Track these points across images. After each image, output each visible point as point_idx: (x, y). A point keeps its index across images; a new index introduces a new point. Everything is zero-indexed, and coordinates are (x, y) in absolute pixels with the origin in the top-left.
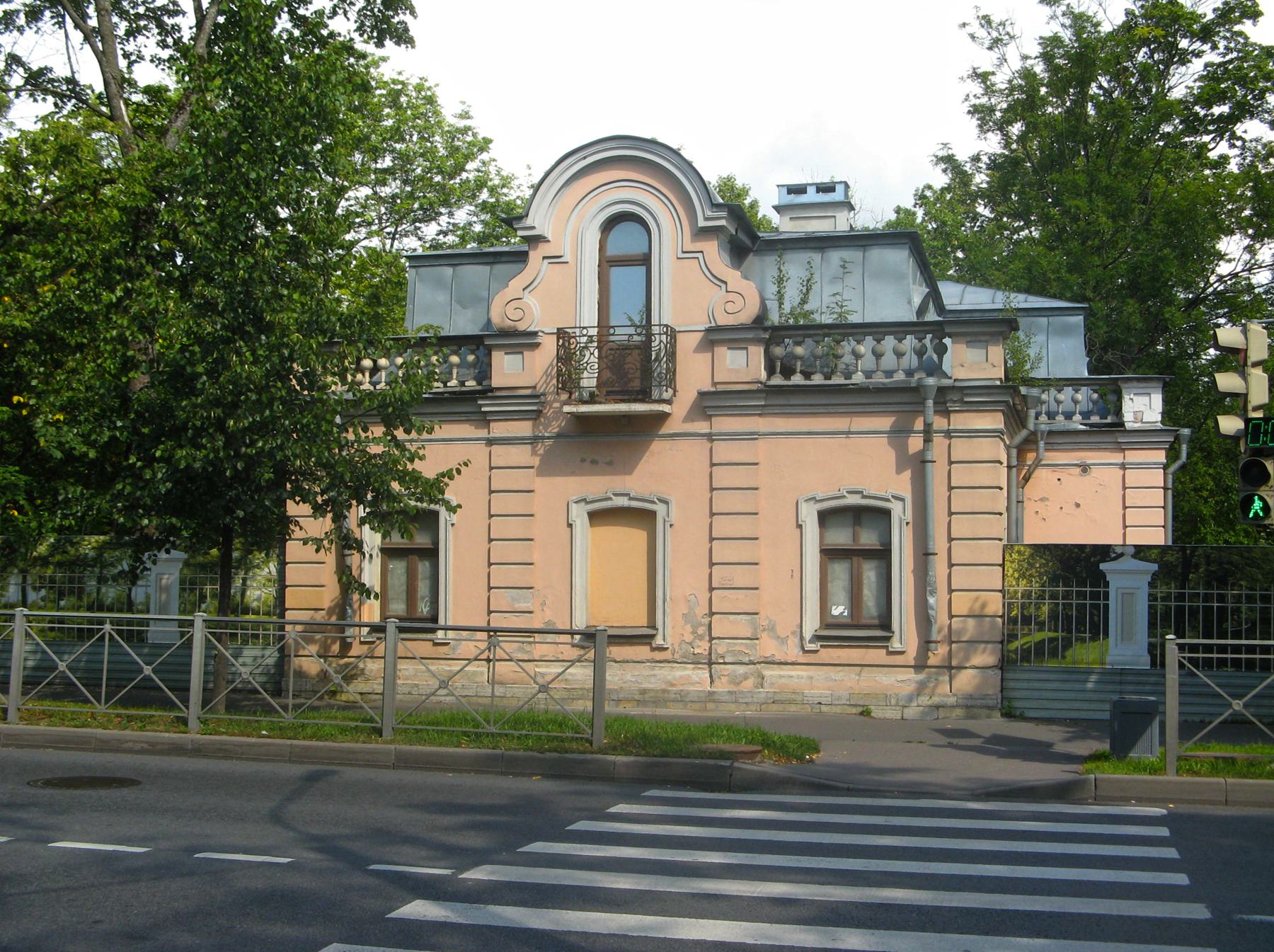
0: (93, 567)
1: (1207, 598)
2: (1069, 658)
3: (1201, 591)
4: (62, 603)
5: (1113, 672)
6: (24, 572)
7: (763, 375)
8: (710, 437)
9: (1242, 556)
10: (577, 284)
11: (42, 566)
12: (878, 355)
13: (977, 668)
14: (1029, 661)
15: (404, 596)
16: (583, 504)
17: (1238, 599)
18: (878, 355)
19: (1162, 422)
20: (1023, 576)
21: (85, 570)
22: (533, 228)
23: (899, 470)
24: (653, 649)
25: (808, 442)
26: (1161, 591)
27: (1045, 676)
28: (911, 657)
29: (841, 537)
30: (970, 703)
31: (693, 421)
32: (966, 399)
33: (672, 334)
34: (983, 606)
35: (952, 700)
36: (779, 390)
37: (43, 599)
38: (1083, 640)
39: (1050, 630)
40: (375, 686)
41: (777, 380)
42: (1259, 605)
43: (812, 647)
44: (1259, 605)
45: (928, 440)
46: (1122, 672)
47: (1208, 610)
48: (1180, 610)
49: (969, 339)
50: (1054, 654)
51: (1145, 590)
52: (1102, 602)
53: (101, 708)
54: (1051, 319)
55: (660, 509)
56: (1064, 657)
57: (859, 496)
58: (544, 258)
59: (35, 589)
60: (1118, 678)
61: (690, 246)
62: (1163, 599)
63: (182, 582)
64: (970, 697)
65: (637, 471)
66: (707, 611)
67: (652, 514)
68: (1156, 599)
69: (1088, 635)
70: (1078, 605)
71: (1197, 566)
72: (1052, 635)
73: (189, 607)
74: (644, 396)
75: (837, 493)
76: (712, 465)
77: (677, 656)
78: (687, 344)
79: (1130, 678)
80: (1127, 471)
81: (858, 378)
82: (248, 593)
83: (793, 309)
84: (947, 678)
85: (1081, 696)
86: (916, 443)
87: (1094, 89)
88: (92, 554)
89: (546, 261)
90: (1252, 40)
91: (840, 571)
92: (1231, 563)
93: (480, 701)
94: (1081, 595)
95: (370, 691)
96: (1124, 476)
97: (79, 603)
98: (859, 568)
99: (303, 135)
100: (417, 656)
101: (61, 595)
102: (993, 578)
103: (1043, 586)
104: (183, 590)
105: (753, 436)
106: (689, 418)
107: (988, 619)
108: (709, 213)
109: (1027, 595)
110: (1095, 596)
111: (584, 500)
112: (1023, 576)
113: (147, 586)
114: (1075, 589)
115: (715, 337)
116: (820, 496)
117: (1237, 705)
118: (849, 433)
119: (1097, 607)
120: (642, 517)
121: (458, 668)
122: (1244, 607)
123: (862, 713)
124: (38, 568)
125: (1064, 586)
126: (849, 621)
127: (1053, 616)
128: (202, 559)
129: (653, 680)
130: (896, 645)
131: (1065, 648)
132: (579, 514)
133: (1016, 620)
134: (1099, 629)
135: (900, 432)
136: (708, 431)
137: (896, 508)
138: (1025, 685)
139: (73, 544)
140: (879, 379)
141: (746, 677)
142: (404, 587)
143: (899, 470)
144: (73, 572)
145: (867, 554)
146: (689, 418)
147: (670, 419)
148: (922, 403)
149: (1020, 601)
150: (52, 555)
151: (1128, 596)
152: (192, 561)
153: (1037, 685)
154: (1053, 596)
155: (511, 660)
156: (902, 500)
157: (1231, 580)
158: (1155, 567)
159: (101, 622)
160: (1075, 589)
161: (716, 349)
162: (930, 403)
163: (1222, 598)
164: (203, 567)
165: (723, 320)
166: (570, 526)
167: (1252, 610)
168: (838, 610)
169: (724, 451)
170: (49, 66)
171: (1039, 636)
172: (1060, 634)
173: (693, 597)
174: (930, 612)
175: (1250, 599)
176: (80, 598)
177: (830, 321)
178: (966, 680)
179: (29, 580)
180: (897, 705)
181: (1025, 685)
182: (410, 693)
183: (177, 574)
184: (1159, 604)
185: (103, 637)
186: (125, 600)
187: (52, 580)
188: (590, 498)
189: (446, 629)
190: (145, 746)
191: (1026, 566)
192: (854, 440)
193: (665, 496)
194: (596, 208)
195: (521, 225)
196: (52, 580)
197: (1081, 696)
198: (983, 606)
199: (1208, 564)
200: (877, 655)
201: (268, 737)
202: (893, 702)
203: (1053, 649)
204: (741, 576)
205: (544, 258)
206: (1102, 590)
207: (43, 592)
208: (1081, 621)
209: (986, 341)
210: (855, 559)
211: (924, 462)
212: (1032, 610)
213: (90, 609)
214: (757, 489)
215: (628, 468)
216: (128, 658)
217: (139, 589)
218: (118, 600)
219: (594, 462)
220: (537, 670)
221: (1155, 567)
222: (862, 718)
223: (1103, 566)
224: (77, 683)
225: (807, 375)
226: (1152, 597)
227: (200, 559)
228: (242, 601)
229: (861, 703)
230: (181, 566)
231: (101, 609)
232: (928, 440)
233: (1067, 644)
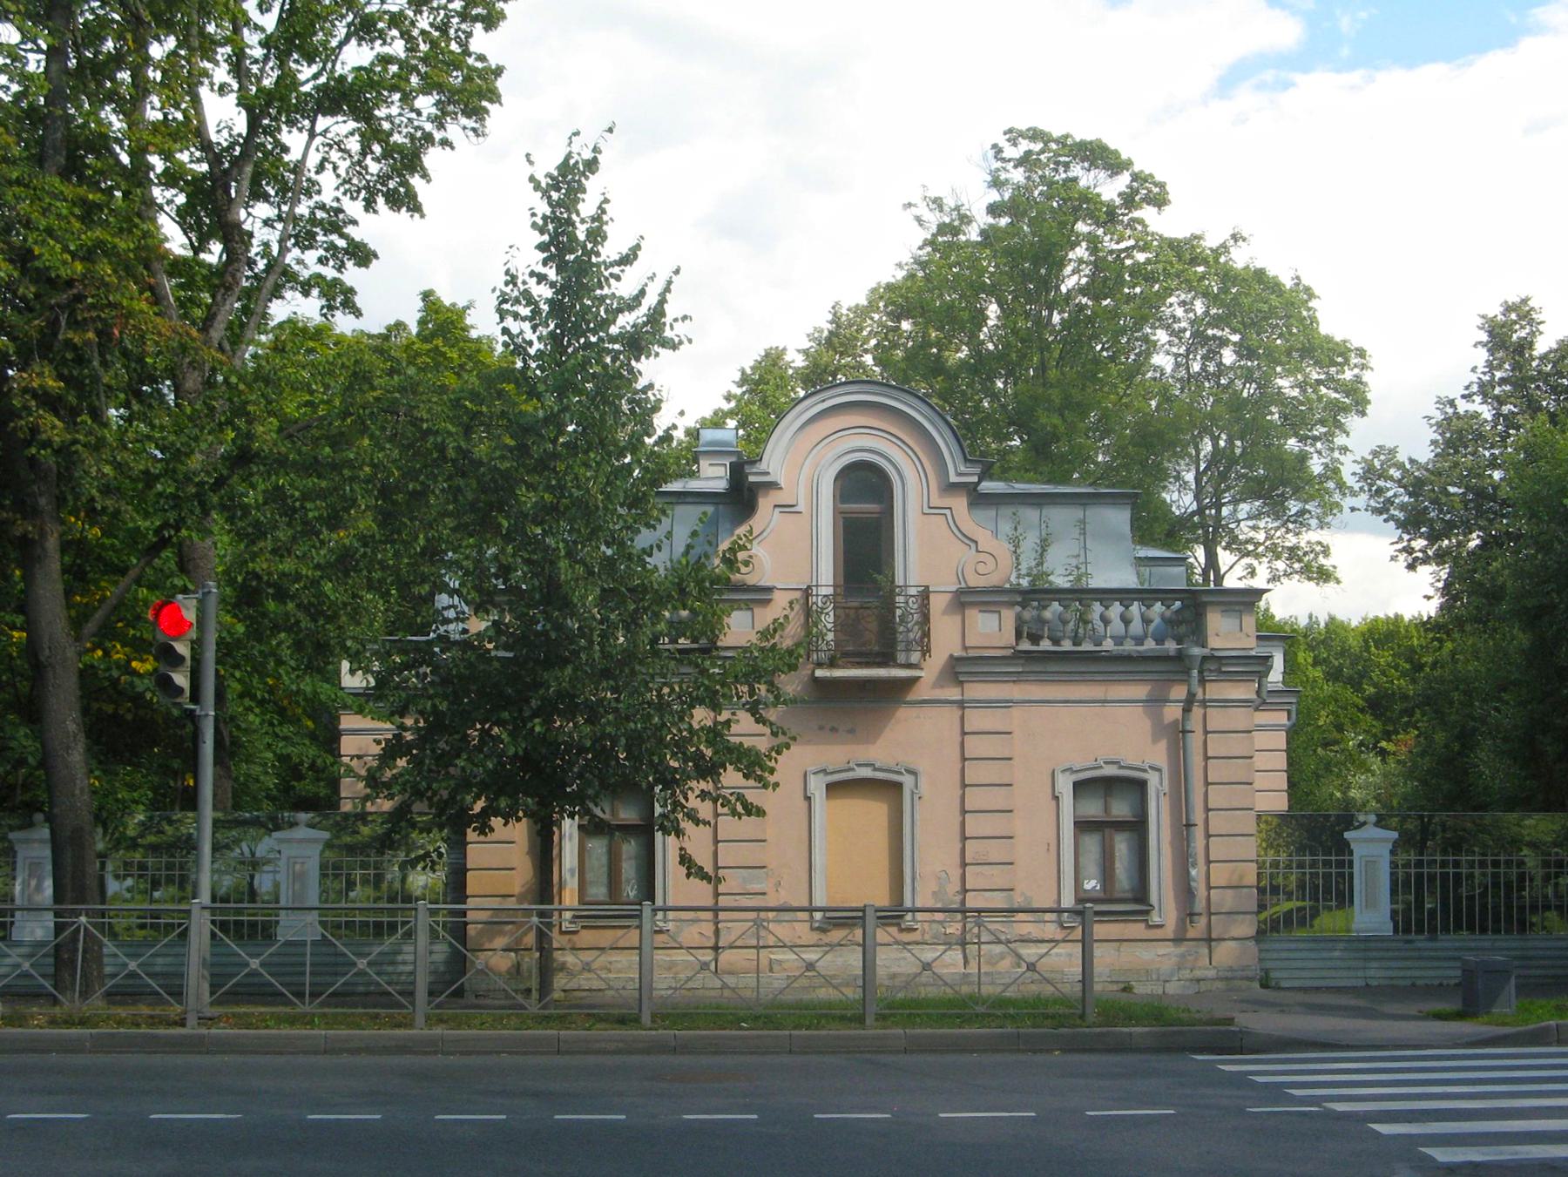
2: (1316, 927)
3: (1438, 858)
4: (157, 894)
5: (1359, 939)
7: (1013, 641)
8: (961, 704)
9: (1474, 823)
10: (813, 538)
11: (127, 849)
12: (1126, 621)
13: (1234, 939)
14: (1278, 932)
15: (604, 879)
16: (821, 775)
17: (1471, 864)
18: (1126, 621)
19: (1284, 682)
20: (1270, 846)
21: (188, 853)
22: (768, 473)
23: (1155, 740)
24: (901, 930)
25: (1063, 710)
26: (1402, 858)
27: (1293, 946)
28: (1169, 931)
29: (1093, 809)
30: (1229, 974)
31: (942, 687)
32: (1224, 669)
33: (925, 595)
34: (1241, 877)
35: (1211, 973)
36: (1028, 656)
37: (129, 890)
38: (1330, 909)
39: (1297, 899)
40: (582, 982)
41: (1026, 645)
42: (1490, 870)
43: (573, 928)
44: (1490, 870)
45: (1187, 710)
46: (1367, 939)
47: (1445, 876)
48: (1420, 876)
49: (1224, 608)
50: (1302, 923)
51: (1387, 857)
52: (1347, 871)
54: (1154, 569)
55: (907, 780)
56: (1312, 926)
57: (1115, 766)
58: (776, 506)
59: (117, 877)
60: (1362, 946)
61: (935, 501)
62: (1404, 866)
64: (1231, 969)
65: (878, 742)
66: (958, 888)
67: (898, 786)
68: (1397, 867)
69: (1334, 903)
70: (1493, 873)
71: (1434, 834)
72: (1299, 904)
73: (332, 896)
74: (887, 659)
75: (1092, 763)
76: (964, 733)
77: (927, 937)
78: (938, 603)
79: (1372, 945)
80: (967, 711)
81: (1108, 645)
82: (410, 879)
83: (1030, 568)
84: (1206, 951)
85: (1329, 963)
86: (1173, 712)
87: (74, 61)
89: (778, 510)
91: (1092, 843)
92: (1464, 830)
93: (708, 993)
94: (1327, 864)
95: (576, 987)
96: (962, 718)
97: (181, 894)
98: (1112, 840)
100: (685, 945)
101: (155, 884)
102: (1249, 848)
103: (1290, 855)
104: (324, 876)
105: (1008, 704)
106: (939, 683)
107: (1245, 890)
108: (962, 468)
109: (1275, 864)
110: (1340, 864)
111: (824, 771)
112: (1270, 846)
113: (275, 872)
114: (1321, 858)
115: (965, 599)
116: (1077, 767)
118: (1105, 701)
119: (1457, 876)
120: (887, 789)
121: (1045, 951)
122: (1477, 872)
123: (1124, 990)
124: (121, 852)
125: (1311, 855)
126: (1102, 895)
127: (1301, 886)
128: (349, 839)
129: (902, 963)
130: (1155, 918)
131: (1313, 917)
132: (817, 786)
133: (1268, 890)
134: (1344, 898)
135: (1156, 701)
136: (959, 698)
137: (1153, 780)
138: (1275, 955)
139: (170, 822)
140: (1129, 647)
141: (1002, 957)
142: (605, 869)
143: (1155, 740)
144: (173, 856)
145: (1119, 825)
146: (939, 683)
147: (918, 684)
148: (1187, 672)
149: (1268, 871)
150: (142, 836)
151: (1370, 864)
152: (336, 842)
153: (1285, 955)
154: (1301, 865)
155: (681, 948)
156: (1159, 770)
157: (1465, 847)
158: (1395, 835)
160: (1321, 858)
161: (967, 612)
162: (1195, 673)
164: (351, 849)
165: (974, 581)
166: (808, 799)
167: (1484, 875)
168: (1091, 884)
169: (976, 719)
171: (1287, 906)
172: (1307, 903)
173: (943, 874)
174: (1193, 884)
175: (1482, 864)
177: (1067, 585)
178: (1226, 953)
179: (110, 867)
180: (1158, 980)
181: (1275, 955)
182: (624, 988)
184: (1400, 871)
186: (246, 890)
187: (142, 866)
188: (830, 769)
189: (914, 910)
190: (621, 1045)
191: (1273, 835)
192: (1109, 710)
193: (912, 767)
194: (830, 455)
195: (755, 470)
196: (142, 866)
197: (1329, 963)
198: (1241, 877)
199: (1444, 831)
200: (1136, 929)
201: (747, 1029)
202: (1154, 977)
203: (1302, 919)
204: (995, 851)
205: (776, 506)
206: (1347, 858)
207: (129, 882)
208: (1327, 891)
209: (1241, 611)
210: (1107, 831)
211: (1184, 732)
212: (1281, 879)
214: (1010, 759)
215: (871, 737)
216: (236, 960)
217: (264, 875)
218: (236, 890)
219: (834, 730)
220: (772, 957)
221: (1395, 835)
222: (1125, 994)
223: (1347, 835)
224: (161, 991)
225: (1056, 642)
226: (1394, 865)
227: (347, 839)
228: (403, 888)
229: (1122, 979)
230: (321, 847)
232: (1187, 710)
233: (1315, 913)
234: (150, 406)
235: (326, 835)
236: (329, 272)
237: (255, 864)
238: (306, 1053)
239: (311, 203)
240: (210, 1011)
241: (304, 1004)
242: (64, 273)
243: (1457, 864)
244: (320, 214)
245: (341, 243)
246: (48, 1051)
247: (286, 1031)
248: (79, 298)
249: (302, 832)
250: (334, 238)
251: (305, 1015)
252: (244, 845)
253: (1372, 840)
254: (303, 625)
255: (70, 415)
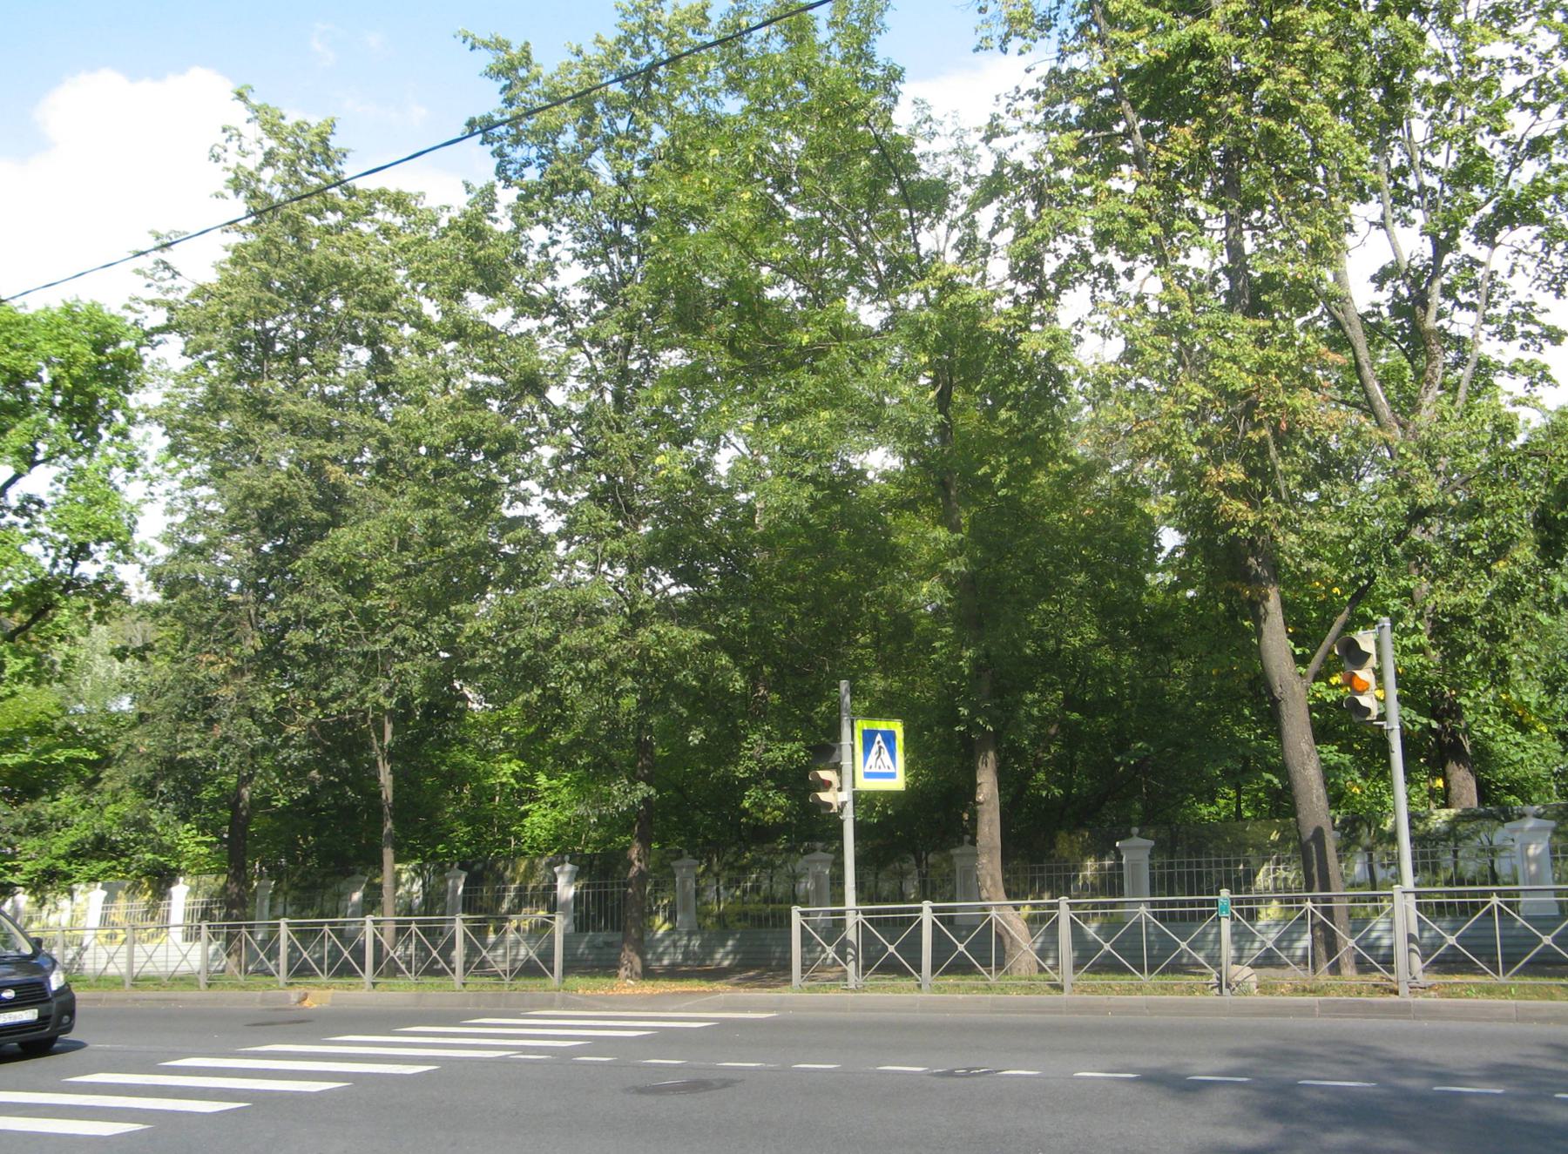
0: (1446, 840)
1: (1189, 865)
6: (1369, 850)
26: (1157, 862)
44: (1223, 869)
47: (1190, 874)
53: (1145, 978)
59: (1383, 866)
63: (1553, 851)
88: (1444, 827)
90: (36, 469)
94: (1189, 865)
99: (1285, 22)
117: (1547, 940)
119: (1199, 874)
122: (1213, 870)
151: (1135, 866)
158: (1152, 843)
159: (410, 922)
163: (1199, 865)
170: (502, 37)
175: (1218, 864)
176: (1435, 873)
183: (1546, 844)
184: (1157, 871)
185: (1490, 913)
213: (1448, 883)
218: (1480, 873)
221: (1152, 843)
226: (1152, 867)
230: (1549, 835)
231: (1461, 882)
234: (1337, 484)
235: (1552, 824)
236: (1527, 356)
237: (1493, 851)
238: (1499, 1020)
239: (1509, 303)
240: (1423, 979)
241: (1497, 973)
242: (1239, 386)
243: (1199, 865)
244: (1516, 310)
245: (1535, 330)
246: (1287, 1015)
247: (1483, 1000)
248: (1255, 405)
249: (819, 855)
250: (1529, 327)
251: (1504, 985)
252: (1482, 835)
253: (1138, 848)
254: (1479, 646)
255: (1254, 501)
